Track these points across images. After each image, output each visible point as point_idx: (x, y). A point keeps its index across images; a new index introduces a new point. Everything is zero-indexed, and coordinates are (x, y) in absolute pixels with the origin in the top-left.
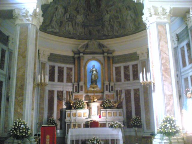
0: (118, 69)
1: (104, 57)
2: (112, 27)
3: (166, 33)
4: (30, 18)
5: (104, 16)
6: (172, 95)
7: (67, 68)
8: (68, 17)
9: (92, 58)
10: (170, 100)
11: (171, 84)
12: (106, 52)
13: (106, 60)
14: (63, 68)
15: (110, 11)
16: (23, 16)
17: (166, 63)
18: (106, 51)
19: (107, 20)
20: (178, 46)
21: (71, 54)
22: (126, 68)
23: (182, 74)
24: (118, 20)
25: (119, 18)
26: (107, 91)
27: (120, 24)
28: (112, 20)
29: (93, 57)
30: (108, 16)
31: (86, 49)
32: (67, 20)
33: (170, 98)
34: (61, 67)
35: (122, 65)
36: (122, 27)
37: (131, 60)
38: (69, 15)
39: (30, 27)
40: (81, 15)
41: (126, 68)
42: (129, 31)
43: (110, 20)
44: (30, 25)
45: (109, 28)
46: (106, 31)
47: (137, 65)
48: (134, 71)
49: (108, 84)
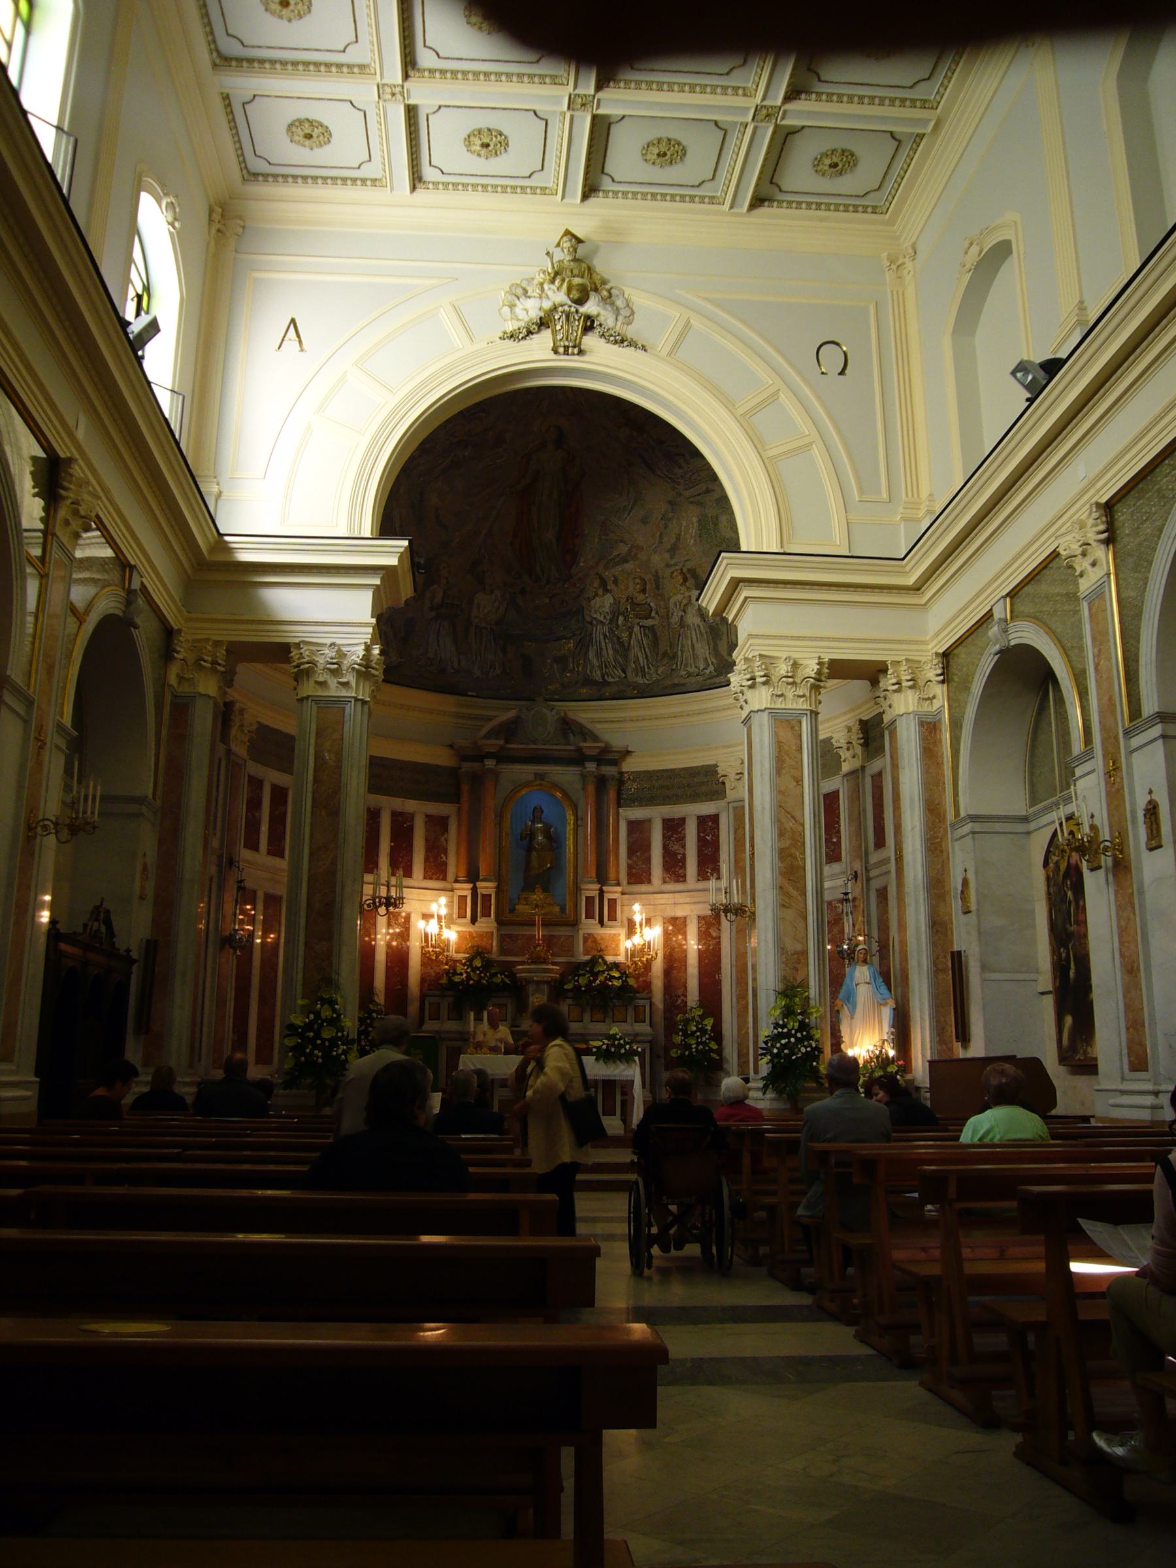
0: (634, 826)
1: (583, 776)
2: (623, 649)
3: (800, 749)
4: (350, 678)
5: (589, 600)
6: (805, 953)
7: (429, 818)
8: (438, 599)
9: (531, 777)
10: (797, 970)
11: (805, 918)
12: (592, 759)
13: (591, 788)
14: (411, 817)
15: (616, 582)
16: (329, 669)
17: (793, 850)
18: (595, 752)
19: (602, 618)
20: (863, 767)
21: (441, 758)
22: (673, 828)
23: (873, 874)
24: (648, 623)
25: (653, 614)
26: (591, 921)
27: (655, 641)
28: (621, 618)
29: (536, 774)
30: (608, 600)
31: (507, 742)
32: (433, 614)
33: (799, 962)
34: (401, 814)
35: (655, 814)
36: (665, 654)
37: (695, 797)
38: (444, 593)
39: (349, 709)
40: (492, 592)
41: (673, 828)
42: (690, 675)
43: (614, 620)
44: (353, 700)
45: (609, 653)
46: (595, 662)
47: (715, 818)
48: (702, 843)
49: (595, 894)
